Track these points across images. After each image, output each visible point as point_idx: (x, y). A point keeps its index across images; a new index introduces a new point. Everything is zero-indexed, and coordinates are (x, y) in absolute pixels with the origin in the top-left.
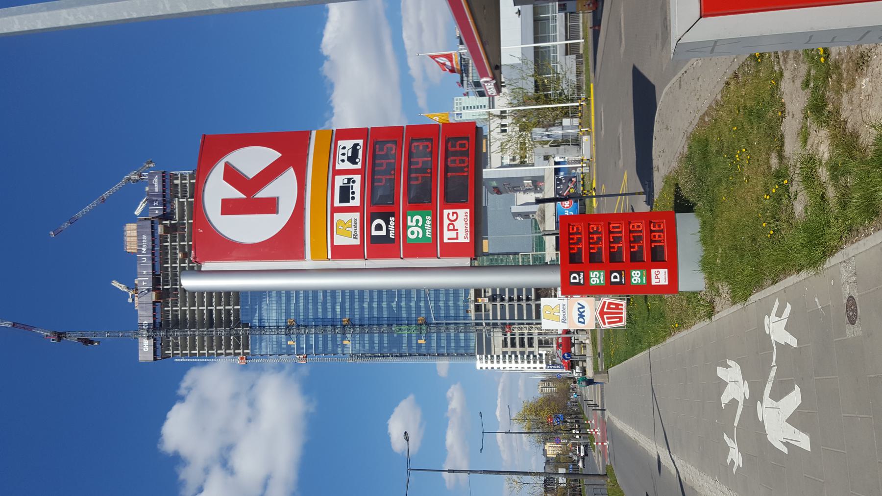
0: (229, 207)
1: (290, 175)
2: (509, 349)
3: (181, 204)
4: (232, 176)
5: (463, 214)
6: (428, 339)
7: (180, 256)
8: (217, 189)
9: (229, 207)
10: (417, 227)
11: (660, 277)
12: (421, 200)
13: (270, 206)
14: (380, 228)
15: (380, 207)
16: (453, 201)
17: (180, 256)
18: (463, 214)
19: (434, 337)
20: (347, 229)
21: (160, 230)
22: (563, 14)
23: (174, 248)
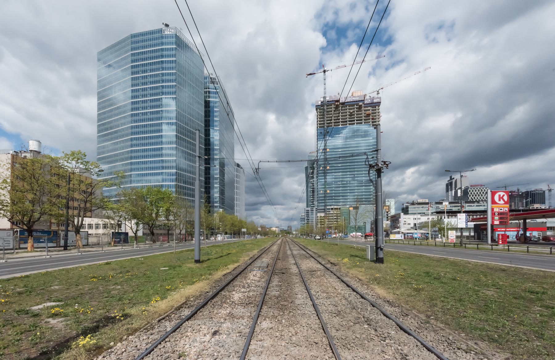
0: (500, 195)
1: (503, 203)
2: (319, 218)
3: (369, 110)
4: (504, 195)
5: (498, 223)
6: (322, 194)
7: (351, 111)
8: (502, 194)
9: (500, 195)
10: (496, 218)
11: (500, 243)
12: (500, 218)
13: (500, 200)
14: (496, 214)
15: (499, 214)
16: (500, 222)
17: (351, 111)
18: (498, 223)
19: (322, 195)
20: (496, 210)
21: (361, 104)
22: (391, 235)
23: (354, 109)
